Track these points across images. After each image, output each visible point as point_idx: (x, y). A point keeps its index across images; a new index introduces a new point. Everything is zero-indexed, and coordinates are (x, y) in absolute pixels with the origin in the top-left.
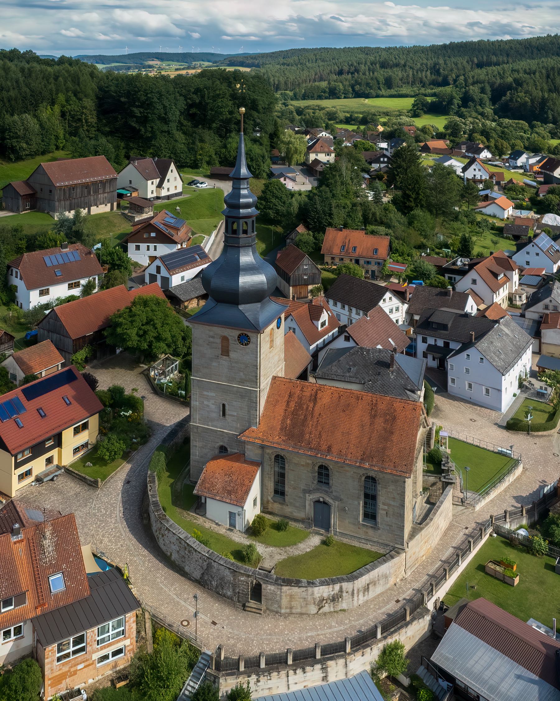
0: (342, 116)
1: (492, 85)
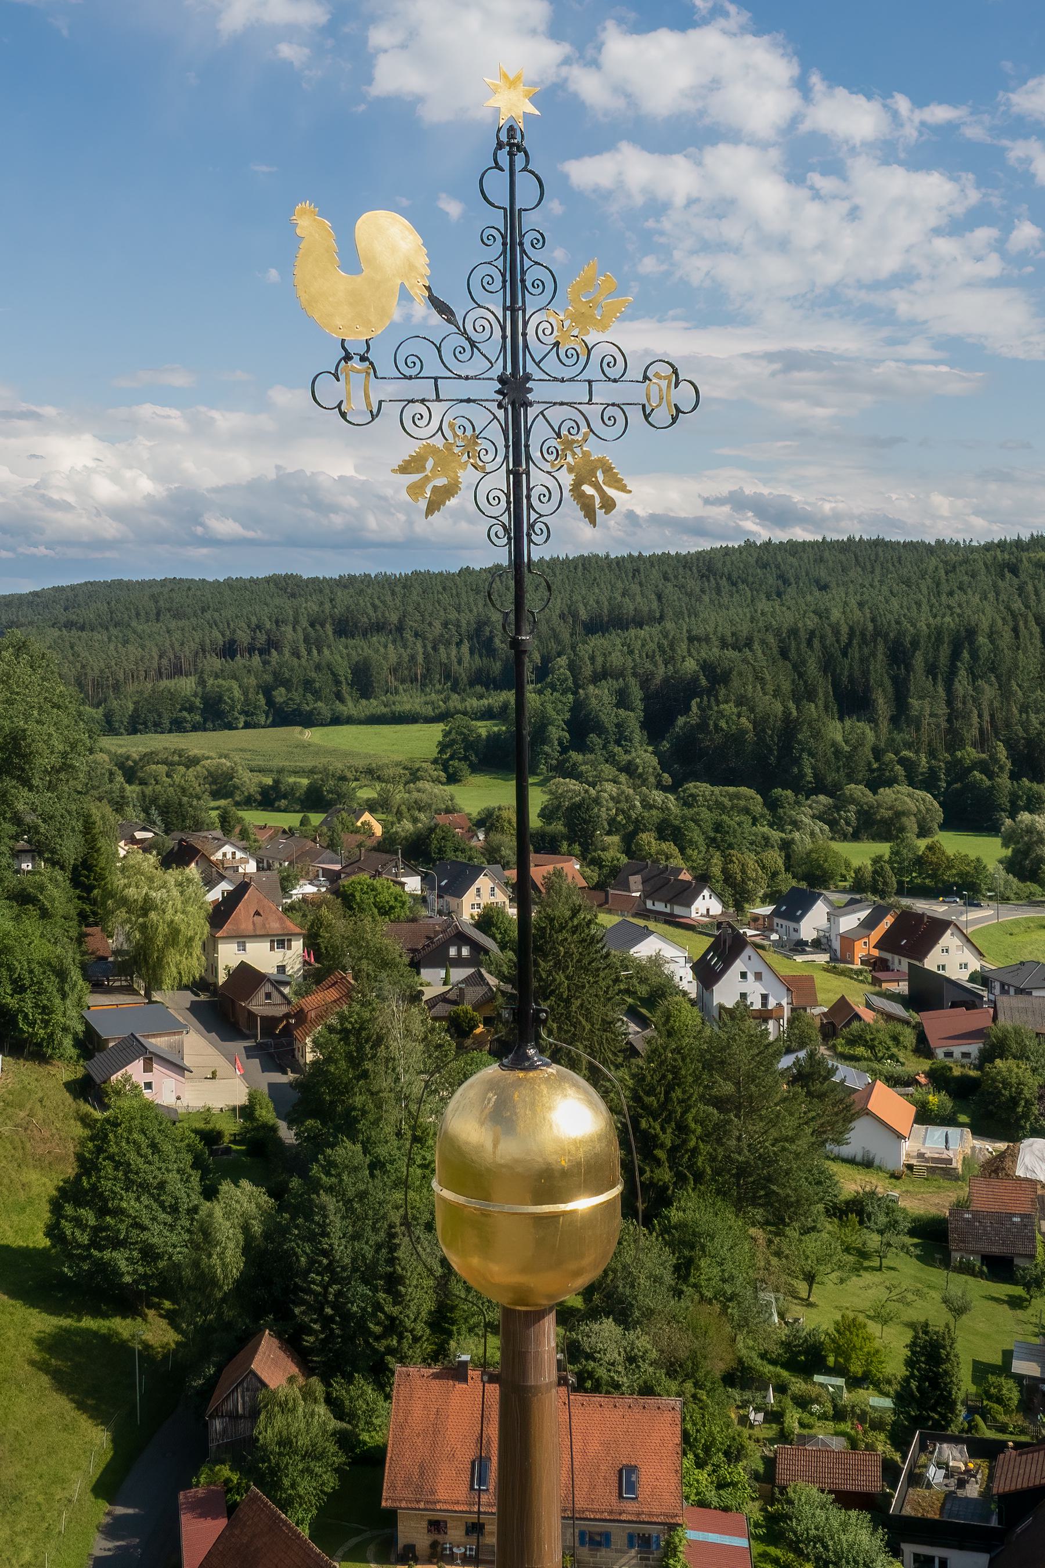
0: (251, 782)
1: (645, 682)
